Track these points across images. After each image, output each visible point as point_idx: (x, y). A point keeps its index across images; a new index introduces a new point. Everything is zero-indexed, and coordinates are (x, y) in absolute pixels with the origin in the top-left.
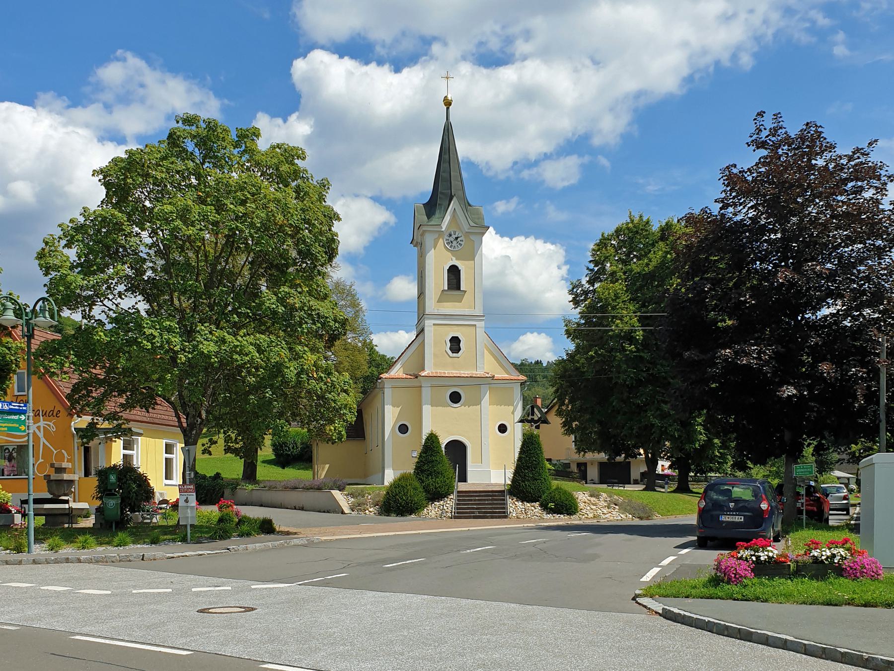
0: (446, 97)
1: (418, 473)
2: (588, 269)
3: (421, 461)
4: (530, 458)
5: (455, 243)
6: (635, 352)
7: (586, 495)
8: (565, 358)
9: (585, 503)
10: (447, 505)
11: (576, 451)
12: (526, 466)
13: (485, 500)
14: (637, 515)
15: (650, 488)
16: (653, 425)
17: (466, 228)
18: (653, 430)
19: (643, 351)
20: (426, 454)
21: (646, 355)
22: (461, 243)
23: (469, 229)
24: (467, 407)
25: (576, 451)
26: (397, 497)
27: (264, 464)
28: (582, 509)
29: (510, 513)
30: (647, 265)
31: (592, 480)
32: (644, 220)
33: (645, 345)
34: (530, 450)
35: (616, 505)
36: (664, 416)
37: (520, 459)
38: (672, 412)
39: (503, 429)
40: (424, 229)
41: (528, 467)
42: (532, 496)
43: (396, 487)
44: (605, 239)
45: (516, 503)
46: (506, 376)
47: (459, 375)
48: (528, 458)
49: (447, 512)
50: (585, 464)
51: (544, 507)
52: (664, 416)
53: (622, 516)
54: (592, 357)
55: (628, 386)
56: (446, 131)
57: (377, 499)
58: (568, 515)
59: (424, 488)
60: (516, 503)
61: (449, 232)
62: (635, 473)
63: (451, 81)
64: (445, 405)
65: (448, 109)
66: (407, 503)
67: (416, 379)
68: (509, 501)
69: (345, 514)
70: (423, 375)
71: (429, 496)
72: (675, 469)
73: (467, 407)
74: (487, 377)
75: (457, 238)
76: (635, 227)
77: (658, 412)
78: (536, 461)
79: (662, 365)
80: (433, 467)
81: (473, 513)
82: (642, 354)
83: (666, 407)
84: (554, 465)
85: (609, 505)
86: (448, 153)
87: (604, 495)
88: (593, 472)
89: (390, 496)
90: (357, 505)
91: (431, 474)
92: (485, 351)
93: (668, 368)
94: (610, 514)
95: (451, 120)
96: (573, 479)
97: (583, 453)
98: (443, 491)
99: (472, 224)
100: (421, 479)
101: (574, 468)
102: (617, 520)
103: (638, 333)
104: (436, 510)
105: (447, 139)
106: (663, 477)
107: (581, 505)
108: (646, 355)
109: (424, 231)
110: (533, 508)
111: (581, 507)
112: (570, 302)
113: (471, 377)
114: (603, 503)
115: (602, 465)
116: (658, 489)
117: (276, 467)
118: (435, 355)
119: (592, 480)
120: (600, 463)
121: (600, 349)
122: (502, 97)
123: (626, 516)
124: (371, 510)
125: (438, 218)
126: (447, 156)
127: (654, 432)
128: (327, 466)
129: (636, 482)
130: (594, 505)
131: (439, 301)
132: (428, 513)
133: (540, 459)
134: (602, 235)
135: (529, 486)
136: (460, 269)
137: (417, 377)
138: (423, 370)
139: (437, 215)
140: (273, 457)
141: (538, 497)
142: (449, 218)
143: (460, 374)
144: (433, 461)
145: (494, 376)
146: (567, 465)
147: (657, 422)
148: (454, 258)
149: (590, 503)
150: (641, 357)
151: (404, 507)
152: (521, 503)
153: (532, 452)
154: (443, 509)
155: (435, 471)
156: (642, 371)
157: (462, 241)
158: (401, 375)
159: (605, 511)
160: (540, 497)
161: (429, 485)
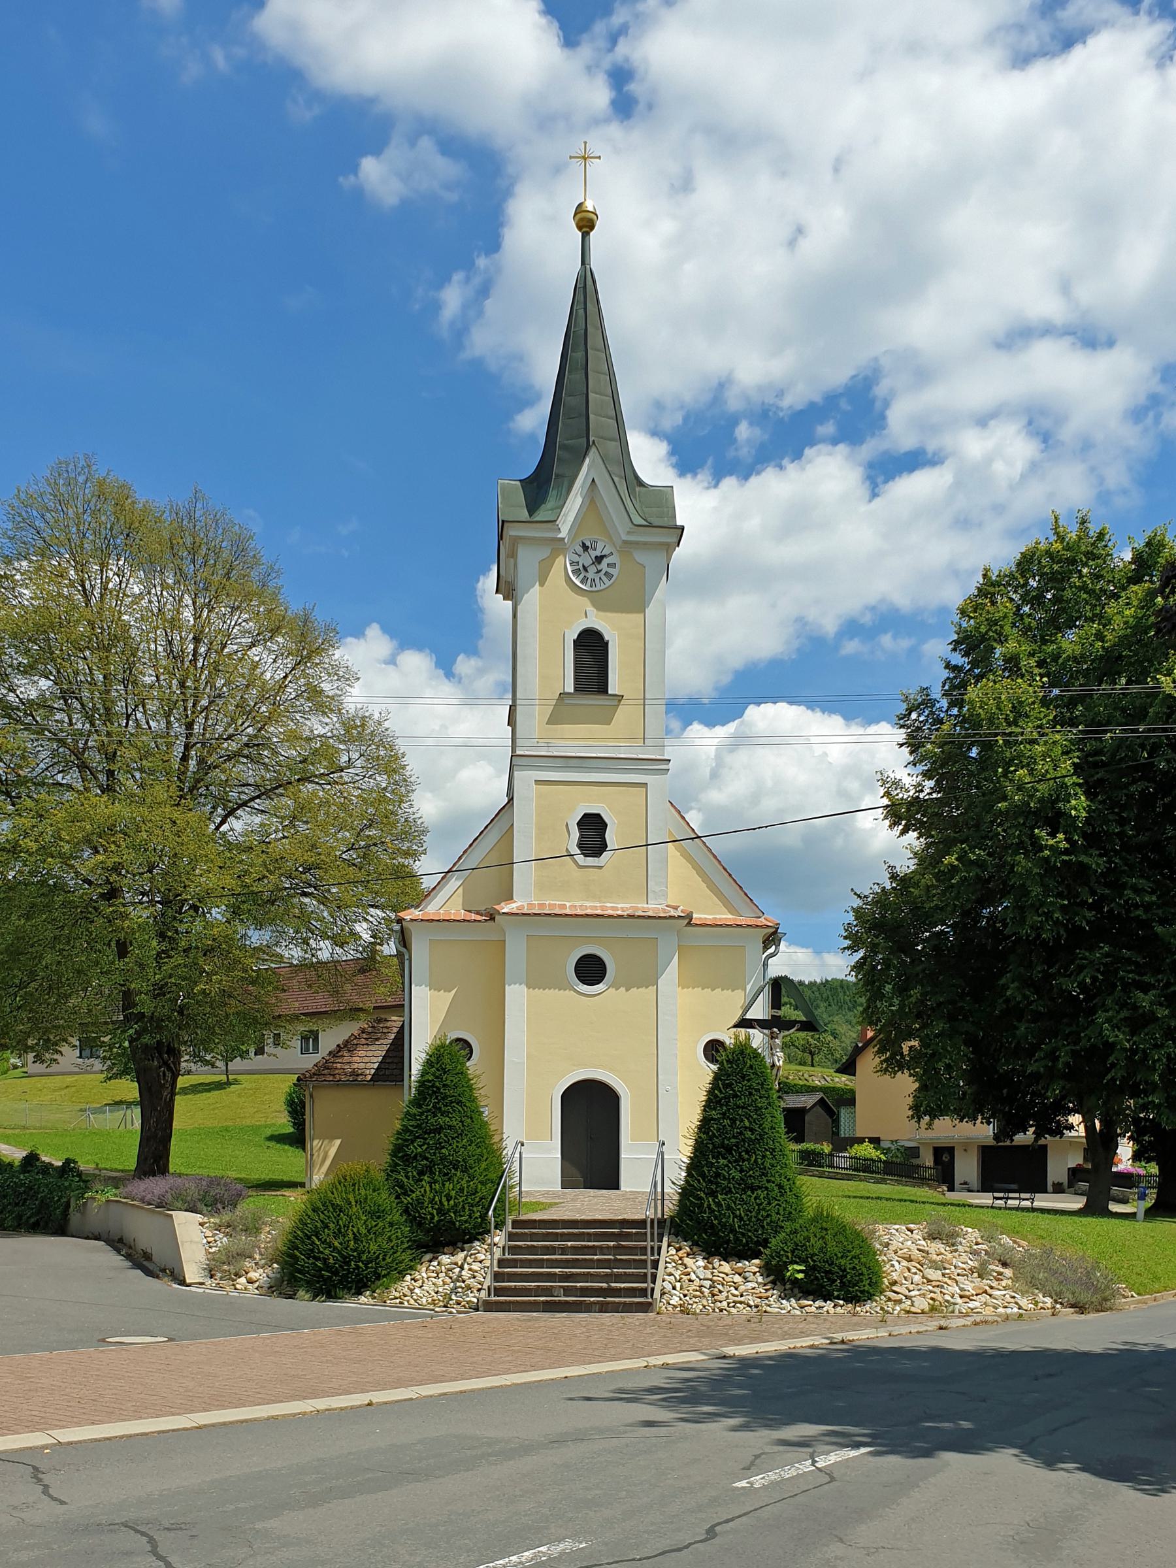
0: (580, 205)
2: (948, 666)
4: (733, 1121)
5: (592, 569)
6: (1066, 852)
7: (917, 1235)
8: (888, 885)
9: (909, 1260)
10: (476, 1266)
11: (910, 1113)
12: (723, 1145)
13: (593, 1250)
14: (1068, 1297)
15: (1096, 1208)
16: (1110, 1047)
17: (622, 530)
18: (1112, 1059)
19: (1085, 850)
20: (420, 1106)
21: (1096, 862)
22: (610, 570)
23: (629, 533)
24: (623, 989)
25: (910, 1113)
28: (895, 1283)
29: (663, 1294)
30: (1100, 636)
31: (965, 1183)
32: (1092, 533)
33: (1093, 837)
34: (735, 1096)
35: (1005, 1265)
36: (1138, 1022)
37: (705, 1124)
38: (1162, 1012)
40: (513, 533)
41: (729, 1150)
42: (737, 1240)
44: (993, 584)
45: (687, 1260)
46: (727, 917)
47: (599, 912)
48: (726, 1122)
49: (469, 1288)
50: (951, 1150)
51: (775, 1274)
52: (1138, 1022)
53: (1024, 1302)
54: (953, 869)
55: (1044, 943)
56: (580, 292)
58: (848, 1300)
59: (406, 1211)
60: (687, 1260)
61: (579, 541)
62: (1057, 1170)
63: (594, 166)
64: (564, 986)
65: (585, 236)
66: (346, 1260)
67: (491, 923)
68: (668, 1253)
69: (183, 1282)
70: (505, 910)
71: (421, 1236)
72: (1148, 1161)
73: (623, 989)
74: (671, 917)
75: (599, 559)
76: (1068, 548)
77: (1125, 1014)
78: (752, 1130)
79: (1137, 890)
81: (548, 1291)
82: (1084, 859)
83: (1145, 1000)
84: (886, 1151)
85: (984, 1264)
86: (582, 347)
87: (972, 1234)
88: (967, 1168)
93: (1154, 898)
94: (984, 1298)
95: (595, 263)
96: (922, 1181)
97: (927, 1118)
98: (462, 1220)
99: (638, 520)
101: (928, 1159)
102: (1007, 1318)
103: (1073, 802)
104: (440, 1282)
105: (581, 312)
106: (1126, 1179)
107: (894, 1269)
108: (1096, 862)
109: (516, 540)
110: (737, 1278)
111: (895, 1276)
112: (902, 745)
113: (630, 916)
114: (964, 1257)
115: (987, 1154)
116: (1114, 1207)
119: (965, 1183)
120: (983, 1146)
121: (972, 848)
122: (787, 402)
123: (1036, 1303)
124: (253, 1275)
125: (552, 510)
126: (580, 354)
127: (1113, 1065)
128: (338, 1142)
129: (1058, 1189)
130: (935, 1266)
131: (553, 720)
132: (412, 1291)
133: (767, 1125)
134: (985, 576)
135: (729, 1208)
136: (606, 638)
137: (492, 919)
138: (510, 898)
139: (551, 502)
140: (290, 1130)
141: (758, 1243)
142: (579, 500)
143: (602, 908)
144: (439, 1130)
145: (689, 917)
146: (914, 1152)
147: (1122, 1038)
148: (591, 609)
149: (925, 1261)
150: (1081, 864)
151: (336, 1273)
152: (701, 1263)
153: (740, 1102)
155: (443, 1158)
156: (1084, 903)
158: (456, 911)
159: (969, 1288)
160: (765, 1243)
161: (420, 1202)
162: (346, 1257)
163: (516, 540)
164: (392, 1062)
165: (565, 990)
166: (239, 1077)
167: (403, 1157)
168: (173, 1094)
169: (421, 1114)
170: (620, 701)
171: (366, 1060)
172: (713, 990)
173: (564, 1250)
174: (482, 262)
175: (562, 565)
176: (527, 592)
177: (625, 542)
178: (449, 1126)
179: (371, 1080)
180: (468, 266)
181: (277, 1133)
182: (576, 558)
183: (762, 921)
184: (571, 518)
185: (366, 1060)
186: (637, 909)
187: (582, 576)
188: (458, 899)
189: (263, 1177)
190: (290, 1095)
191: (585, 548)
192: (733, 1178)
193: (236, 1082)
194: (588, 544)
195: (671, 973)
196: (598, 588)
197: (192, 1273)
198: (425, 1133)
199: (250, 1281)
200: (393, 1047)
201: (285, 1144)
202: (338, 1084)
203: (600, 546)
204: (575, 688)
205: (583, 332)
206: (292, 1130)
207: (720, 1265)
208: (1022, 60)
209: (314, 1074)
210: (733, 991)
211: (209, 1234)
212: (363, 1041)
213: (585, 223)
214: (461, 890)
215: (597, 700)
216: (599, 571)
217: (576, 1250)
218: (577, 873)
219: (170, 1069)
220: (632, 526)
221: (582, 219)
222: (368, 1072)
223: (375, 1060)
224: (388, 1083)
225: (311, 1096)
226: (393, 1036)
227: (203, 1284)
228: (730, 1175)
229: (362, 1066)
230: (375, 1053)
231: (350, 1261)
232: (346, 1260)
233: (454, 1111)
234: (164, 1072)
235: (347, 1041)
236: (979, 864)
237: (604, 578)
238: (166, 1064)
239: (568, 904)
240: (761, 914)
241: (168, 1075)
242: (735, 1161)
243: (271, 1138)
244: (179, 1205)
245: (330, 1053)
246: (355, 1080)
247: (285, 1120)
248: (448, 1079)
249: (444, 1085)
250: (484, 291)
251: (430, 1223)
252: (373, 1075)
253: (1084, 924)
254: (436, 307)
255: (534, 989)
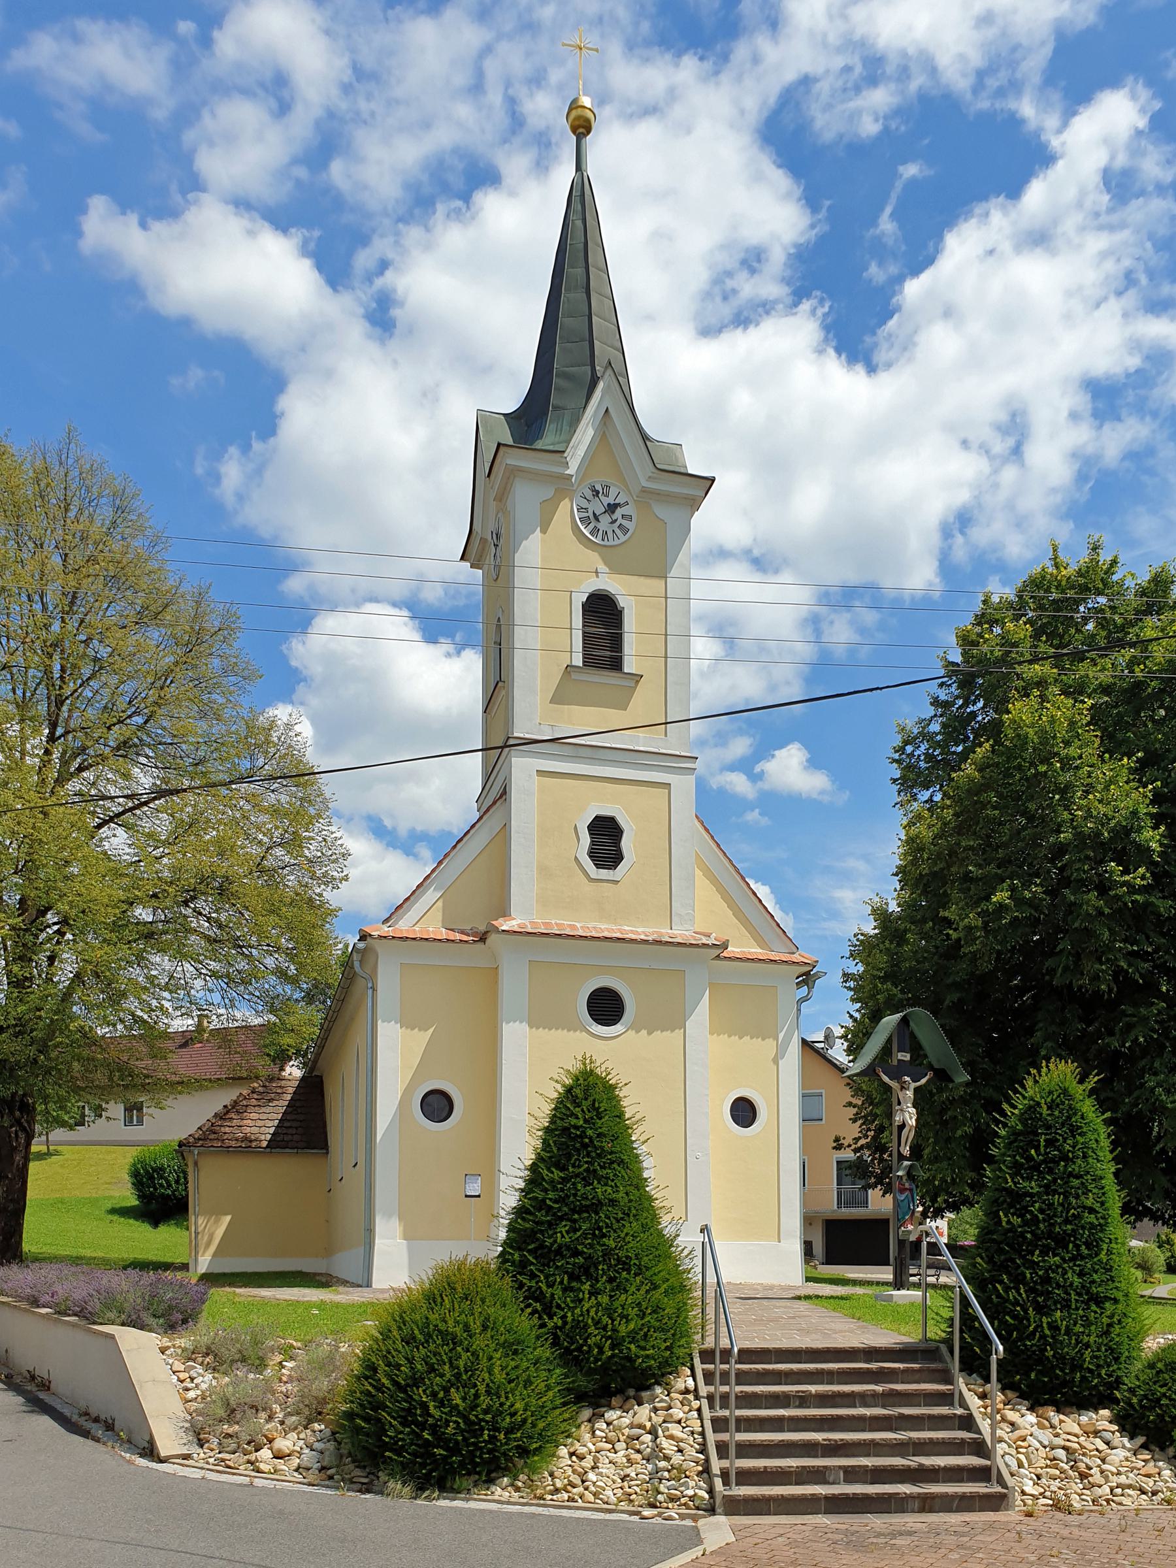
0: (575, 101)
1: (523, 1264)
3: (541, 1205)
5: (605, 520)
12: (1050, 1235)
20: (563, 1169)
24: (644, 1032)
26: (421, 1394)
27: (110, 1217)
34: (1065, 1158)
39: (744, 1112)
43: (409, 1340)
46: (756, 951)
54: (1001, 907)
57: (322, 1385)
59: (556, 1343)
64: (574, 1026)
66: (473, 1428)
67: (480, 946)
70: (504, 928)
71: (582, 1382)
73: (644, 1032)
75: (612, 508)
80: (598, 1233)
86: (582, 263)
89: (380, 1388)
90: (221, 1413)
91: (587, 1271)
92: (698, 873)
95: (591, 170)
98: (646, 1355)
100: (538, 1296)
104: (620, 1457)
105: (579, 223)
109: (514, 472)
117: (137, 1223)
118: (544, 871)
124: (284, 1444)
126: (580, 271)
128: (229, 1218)
131: (558, 699)
138: (505, 913)
142: (591, 432)
144: (596, 1206)
148: (602, 567)
154: (657, 1453)
155: (607, 1253)
157: (629, 518)
158: (435, 928)
162: (473, 1423)
163: (514, 472)
164: (290, 1127)
165: (575, 1031)
166: (59, 1148)
167: (536, 1249)
168: (27, 1160)
169: (564, 1180)
170: (638, 682)
171: (260, 1123)
172: (741, 1038)
173: (804, 1400)
174: (257, 446)
175: (566, 511)
176: (527, 538)
177: (644, 490)
178: (611, 1200)
179: (267, 1147)
180: (246, 448)
181: (118, 1206)
182: (584, 504)
183: (796, 958)
184: (581, 452)
185: (260, 1123)
186: (662, 934)
187: (591, 526)
188: (437, 914)
189: (125, 1256)
190: (134, 1165)
191: (596, 493)
192: (1072, 1284)
193: (57, 1153)
194: (598, 487)
195: (701, 1016)
196: (611, 543)
197: (169, 1440)
198: (574, 1211)
199: (278, 1456)
200: (290, 1110)
201: (130, 1218)
202: (227, 1150)
203: (613, 492)
204: (584, 662)
205: (582, 246)
206: (137, 1203)
207: (1061, 1421)
208: (709, 331)
209: (199, 1139)
210: (763, 1039)
211: (179, 1366)
212: (254, 1102)
213: (581, 122)
214: (440, 903)
215: (607, 678)
216: (614, 522)
217: (824, 1400)
218: (589, 887)
219: (24, 1129)
220: (656, 471)
221: (579, 118)
222: (263, 1137)
223: (270, 1124)
224: (287, 1150)
225: (196, 1164)
226: (289, 1097)
227: (187, 1457)
228: (1065, 1280)
229: (255, 1130)
230: (270, 1116)
231: (482, 1429)
232: (473, 1428)
233: (615, 1175)
234: (16, 1131)
235: (235, 1102)
236: (1033, 903)
237: (618, 531)
238: (18, 1122)
239: (578, 925)
240: (795, 950)
241: (22, 1136)
242: (1071, 1260)
243: (113, 1211)
244: (111, 1315)
245: (216, 1115)
246: (247, 1147)
247: (128, 1193)
248: (604, 1124)
249: (600, 1135)
250: (259, 471)
251: (597, 1360)
252: (269, 1141)
253: (1137, 976)
254: (217, 478)
255: (538, 1028)
